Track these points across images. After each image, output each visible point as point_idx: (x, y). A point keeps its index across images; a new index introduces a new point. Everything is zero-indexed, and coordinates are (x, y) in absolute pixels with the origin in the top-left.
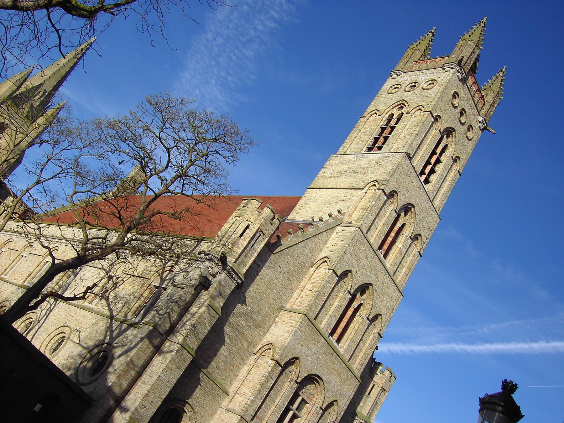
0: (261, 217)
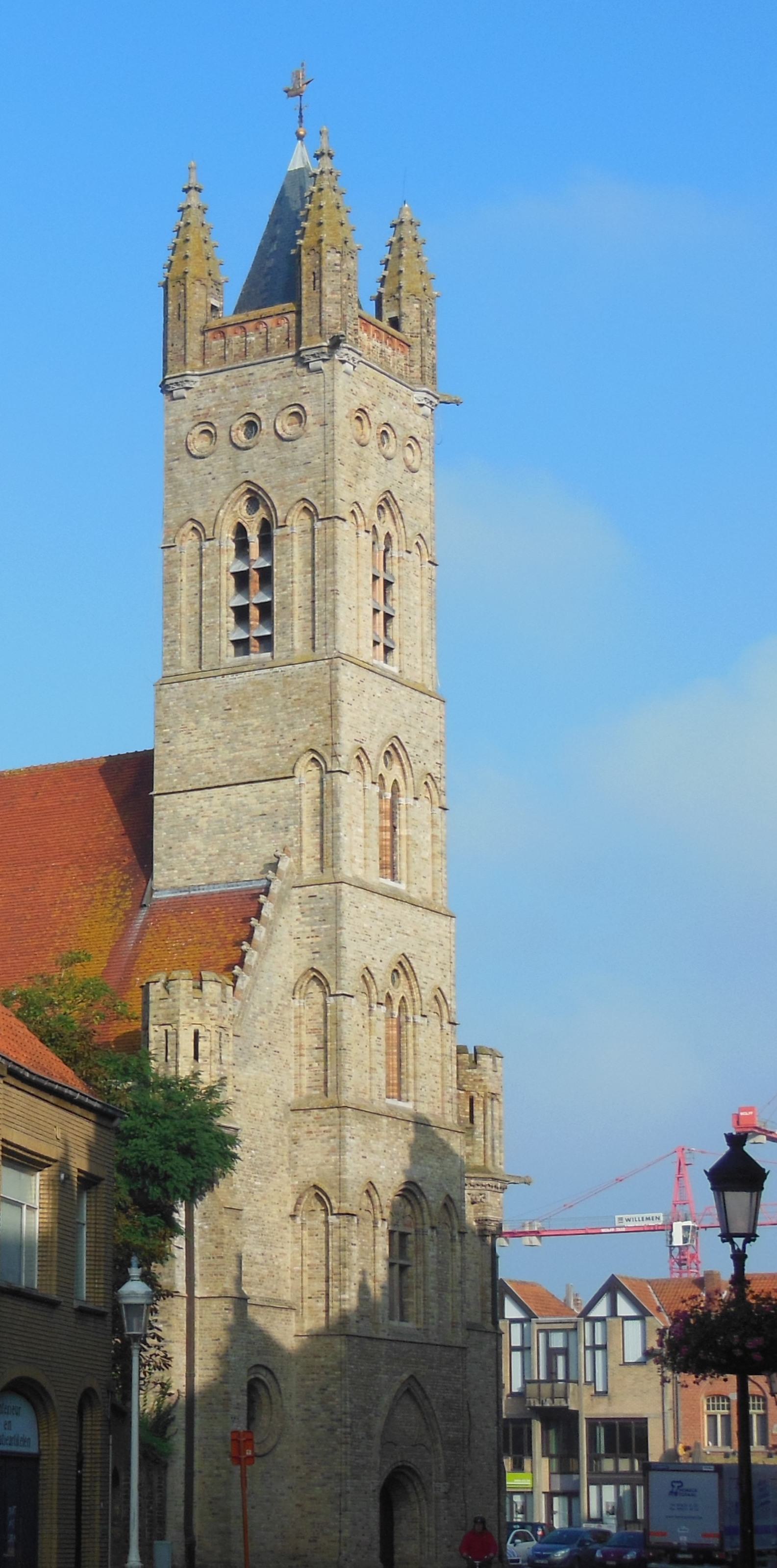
0: (207, 1005)
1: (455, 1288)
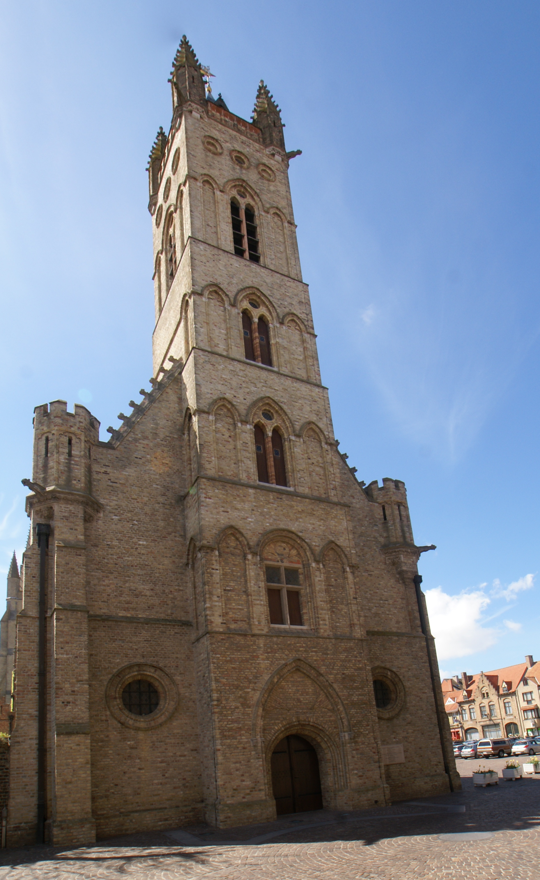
0: (52, 418)
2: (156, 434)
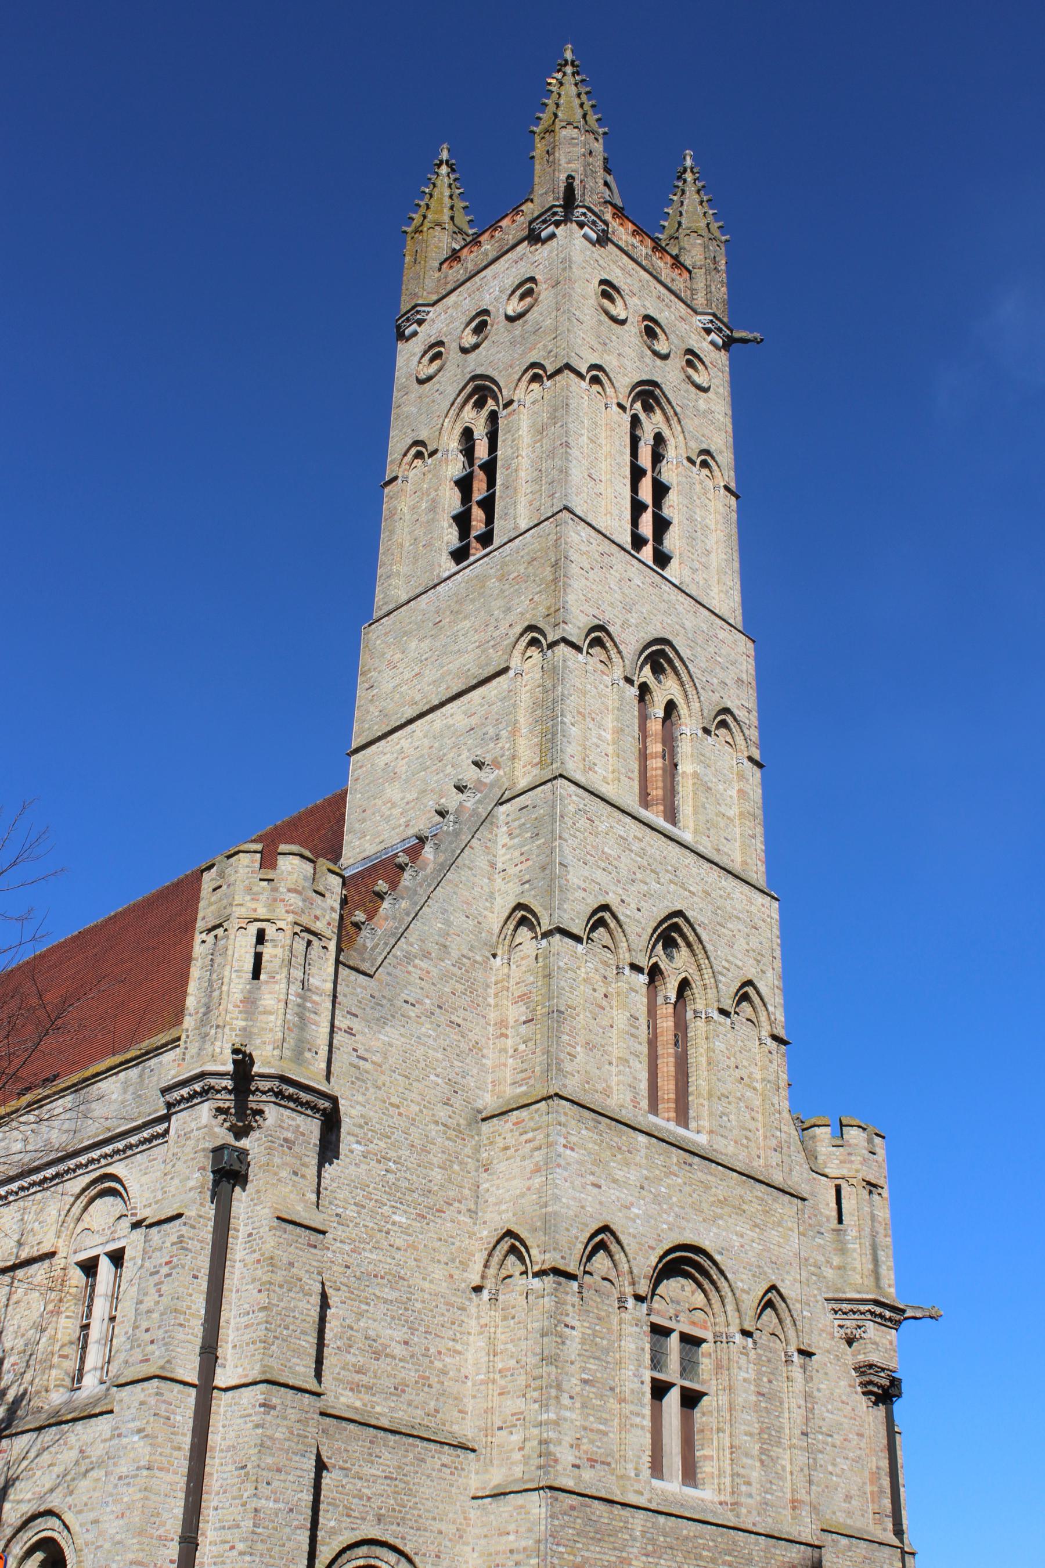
0: (282, 890)
1: (794, 1441)
2: (445, 946)
